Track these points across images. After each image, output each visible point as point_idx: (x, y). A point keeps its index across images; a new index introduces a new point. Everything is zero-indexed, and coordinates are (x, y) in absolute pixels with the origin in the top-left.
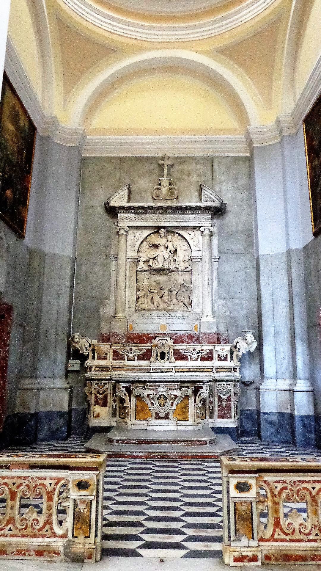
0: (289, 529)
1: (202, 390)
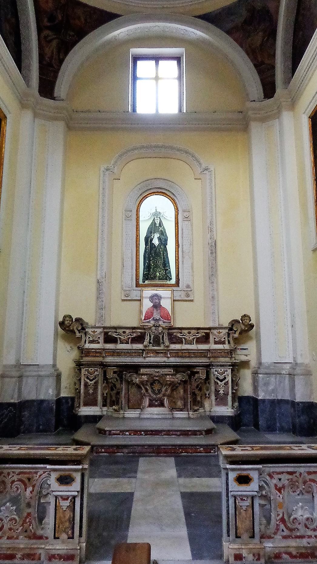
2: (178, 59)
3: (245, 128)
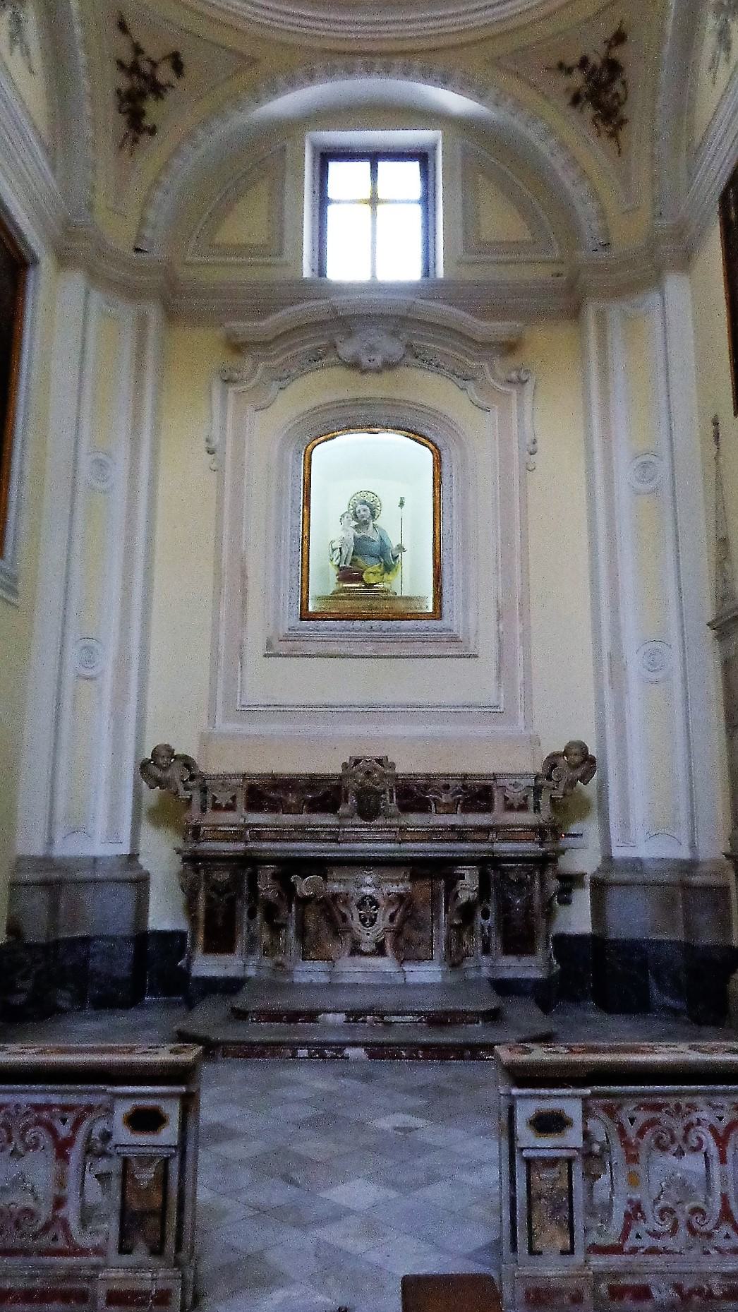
0: (663, 1223)
2: (422, 157)
3: (574, 313)
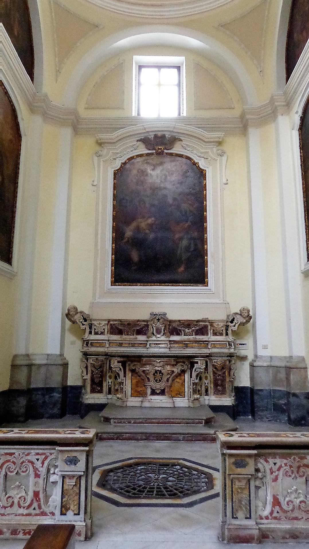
1: (197, 365)
2: (179, 68)
